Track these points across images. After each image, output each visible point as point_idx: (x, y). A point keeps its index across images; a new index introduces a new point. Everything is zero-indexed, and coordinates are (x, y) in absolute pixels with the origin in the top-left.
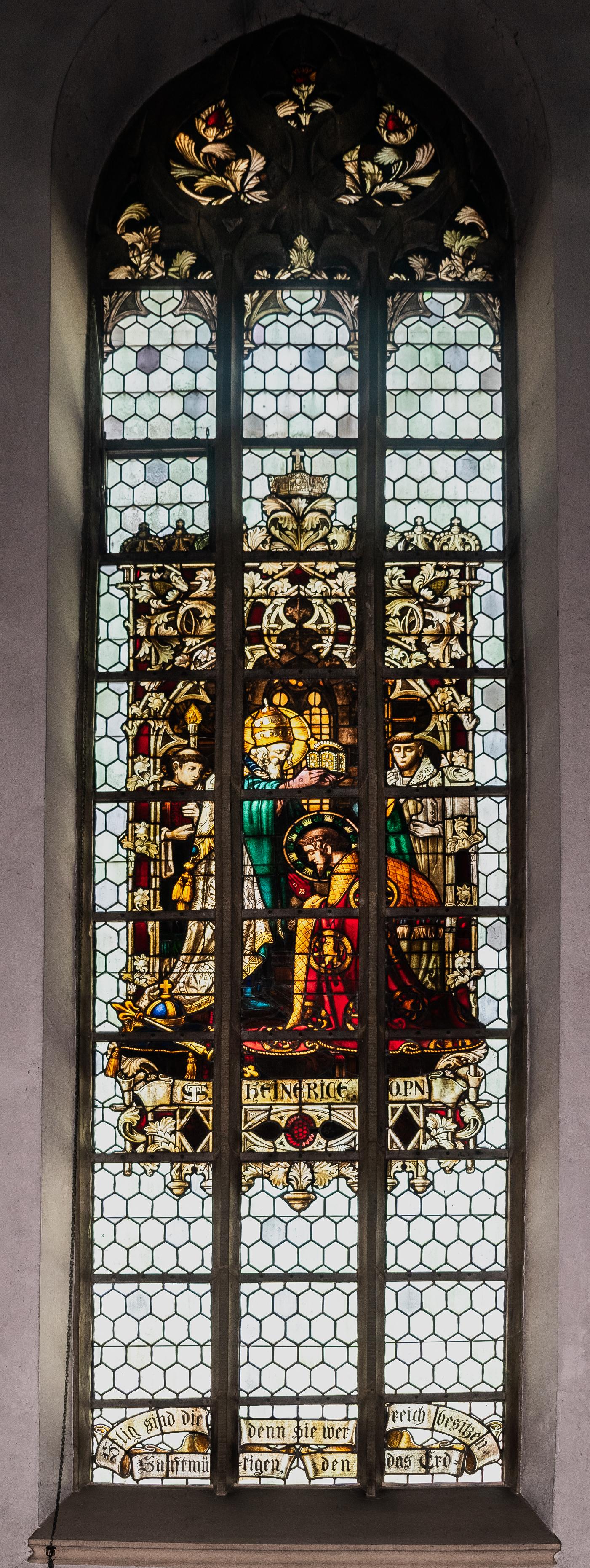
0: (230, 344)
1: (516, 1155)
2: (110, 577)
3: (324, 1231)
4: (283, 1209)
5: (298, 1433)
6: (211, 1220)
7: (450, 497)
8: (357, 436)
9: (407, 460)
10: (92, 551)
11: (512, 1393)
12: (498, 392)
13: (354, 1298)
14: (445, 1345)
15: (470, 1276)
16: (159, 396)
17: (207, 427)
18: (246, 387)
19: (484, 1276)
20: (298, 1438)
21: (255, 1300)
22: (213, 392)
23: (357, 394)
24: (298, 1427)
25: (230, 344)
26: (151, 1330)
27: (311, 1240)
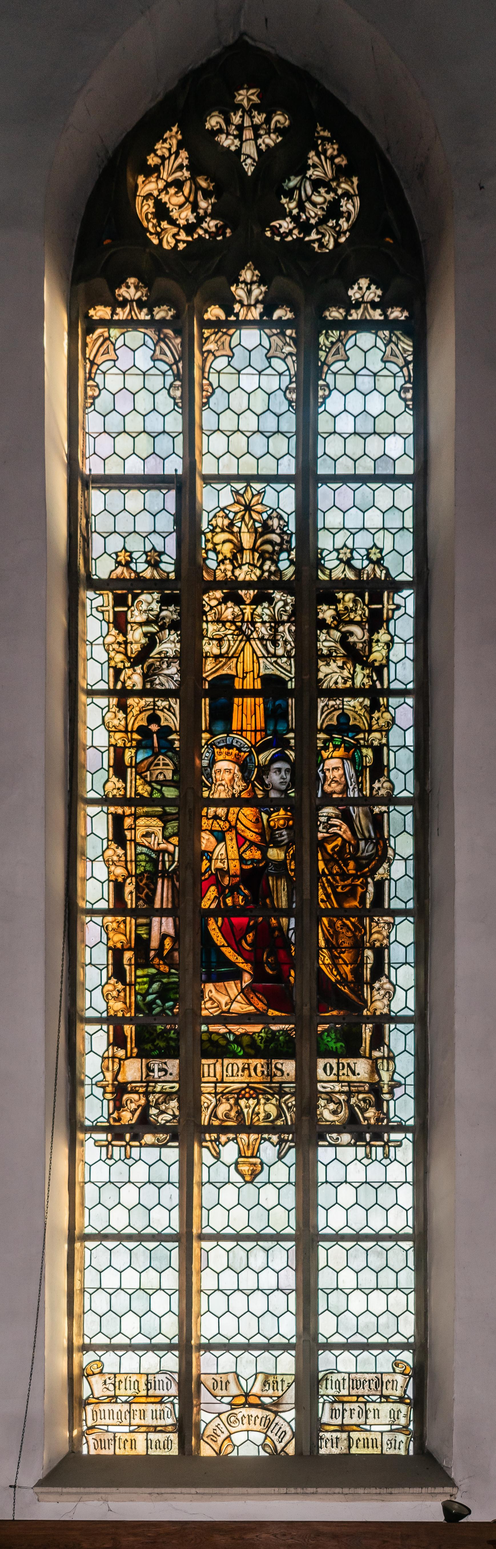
0: (307, 390)
1: (422, 1132)
2: (96, 605)
3: (269, 1195)
4: (235, 1177)
5: (147, 1385)
6: (177, 1185)
7: (366, 526)
8: (319, 473)
9: (394, 491)
10: (77, 580)
11: (421, 1346)
12: (180, 433)
13: (411, 1254)
14: (370, 1302)
15: (367, 1238)
16: (384, 436)
17: (175, 466)
18: (320, 430)
19: (396, 1237)
20: (148, 1390)
21: (330, 1256)
22: (180, 433)
23: (181, 435)
24: (147, 1380)
25: (307, 390)
26: (248, 1280)
27: (279, 1204)
